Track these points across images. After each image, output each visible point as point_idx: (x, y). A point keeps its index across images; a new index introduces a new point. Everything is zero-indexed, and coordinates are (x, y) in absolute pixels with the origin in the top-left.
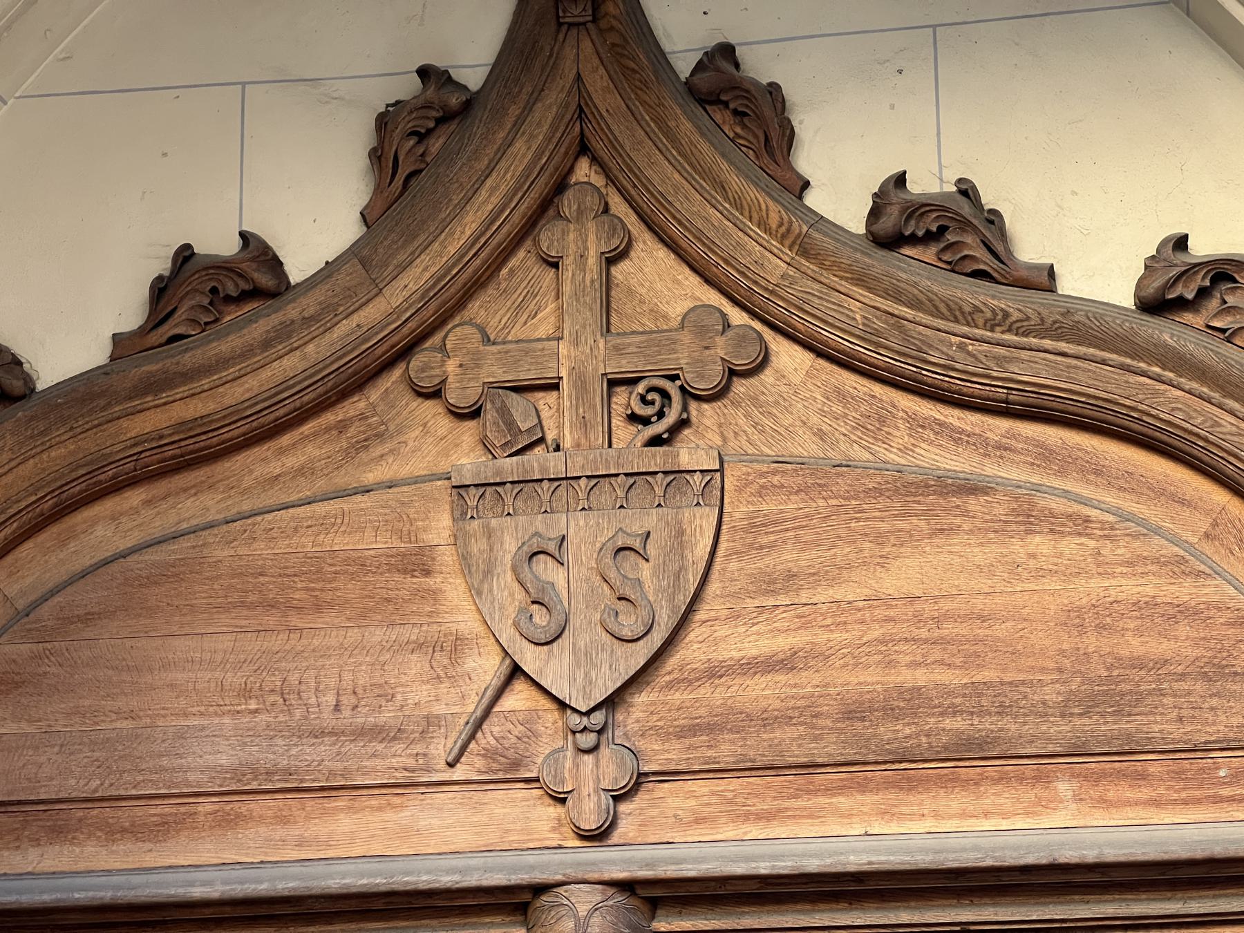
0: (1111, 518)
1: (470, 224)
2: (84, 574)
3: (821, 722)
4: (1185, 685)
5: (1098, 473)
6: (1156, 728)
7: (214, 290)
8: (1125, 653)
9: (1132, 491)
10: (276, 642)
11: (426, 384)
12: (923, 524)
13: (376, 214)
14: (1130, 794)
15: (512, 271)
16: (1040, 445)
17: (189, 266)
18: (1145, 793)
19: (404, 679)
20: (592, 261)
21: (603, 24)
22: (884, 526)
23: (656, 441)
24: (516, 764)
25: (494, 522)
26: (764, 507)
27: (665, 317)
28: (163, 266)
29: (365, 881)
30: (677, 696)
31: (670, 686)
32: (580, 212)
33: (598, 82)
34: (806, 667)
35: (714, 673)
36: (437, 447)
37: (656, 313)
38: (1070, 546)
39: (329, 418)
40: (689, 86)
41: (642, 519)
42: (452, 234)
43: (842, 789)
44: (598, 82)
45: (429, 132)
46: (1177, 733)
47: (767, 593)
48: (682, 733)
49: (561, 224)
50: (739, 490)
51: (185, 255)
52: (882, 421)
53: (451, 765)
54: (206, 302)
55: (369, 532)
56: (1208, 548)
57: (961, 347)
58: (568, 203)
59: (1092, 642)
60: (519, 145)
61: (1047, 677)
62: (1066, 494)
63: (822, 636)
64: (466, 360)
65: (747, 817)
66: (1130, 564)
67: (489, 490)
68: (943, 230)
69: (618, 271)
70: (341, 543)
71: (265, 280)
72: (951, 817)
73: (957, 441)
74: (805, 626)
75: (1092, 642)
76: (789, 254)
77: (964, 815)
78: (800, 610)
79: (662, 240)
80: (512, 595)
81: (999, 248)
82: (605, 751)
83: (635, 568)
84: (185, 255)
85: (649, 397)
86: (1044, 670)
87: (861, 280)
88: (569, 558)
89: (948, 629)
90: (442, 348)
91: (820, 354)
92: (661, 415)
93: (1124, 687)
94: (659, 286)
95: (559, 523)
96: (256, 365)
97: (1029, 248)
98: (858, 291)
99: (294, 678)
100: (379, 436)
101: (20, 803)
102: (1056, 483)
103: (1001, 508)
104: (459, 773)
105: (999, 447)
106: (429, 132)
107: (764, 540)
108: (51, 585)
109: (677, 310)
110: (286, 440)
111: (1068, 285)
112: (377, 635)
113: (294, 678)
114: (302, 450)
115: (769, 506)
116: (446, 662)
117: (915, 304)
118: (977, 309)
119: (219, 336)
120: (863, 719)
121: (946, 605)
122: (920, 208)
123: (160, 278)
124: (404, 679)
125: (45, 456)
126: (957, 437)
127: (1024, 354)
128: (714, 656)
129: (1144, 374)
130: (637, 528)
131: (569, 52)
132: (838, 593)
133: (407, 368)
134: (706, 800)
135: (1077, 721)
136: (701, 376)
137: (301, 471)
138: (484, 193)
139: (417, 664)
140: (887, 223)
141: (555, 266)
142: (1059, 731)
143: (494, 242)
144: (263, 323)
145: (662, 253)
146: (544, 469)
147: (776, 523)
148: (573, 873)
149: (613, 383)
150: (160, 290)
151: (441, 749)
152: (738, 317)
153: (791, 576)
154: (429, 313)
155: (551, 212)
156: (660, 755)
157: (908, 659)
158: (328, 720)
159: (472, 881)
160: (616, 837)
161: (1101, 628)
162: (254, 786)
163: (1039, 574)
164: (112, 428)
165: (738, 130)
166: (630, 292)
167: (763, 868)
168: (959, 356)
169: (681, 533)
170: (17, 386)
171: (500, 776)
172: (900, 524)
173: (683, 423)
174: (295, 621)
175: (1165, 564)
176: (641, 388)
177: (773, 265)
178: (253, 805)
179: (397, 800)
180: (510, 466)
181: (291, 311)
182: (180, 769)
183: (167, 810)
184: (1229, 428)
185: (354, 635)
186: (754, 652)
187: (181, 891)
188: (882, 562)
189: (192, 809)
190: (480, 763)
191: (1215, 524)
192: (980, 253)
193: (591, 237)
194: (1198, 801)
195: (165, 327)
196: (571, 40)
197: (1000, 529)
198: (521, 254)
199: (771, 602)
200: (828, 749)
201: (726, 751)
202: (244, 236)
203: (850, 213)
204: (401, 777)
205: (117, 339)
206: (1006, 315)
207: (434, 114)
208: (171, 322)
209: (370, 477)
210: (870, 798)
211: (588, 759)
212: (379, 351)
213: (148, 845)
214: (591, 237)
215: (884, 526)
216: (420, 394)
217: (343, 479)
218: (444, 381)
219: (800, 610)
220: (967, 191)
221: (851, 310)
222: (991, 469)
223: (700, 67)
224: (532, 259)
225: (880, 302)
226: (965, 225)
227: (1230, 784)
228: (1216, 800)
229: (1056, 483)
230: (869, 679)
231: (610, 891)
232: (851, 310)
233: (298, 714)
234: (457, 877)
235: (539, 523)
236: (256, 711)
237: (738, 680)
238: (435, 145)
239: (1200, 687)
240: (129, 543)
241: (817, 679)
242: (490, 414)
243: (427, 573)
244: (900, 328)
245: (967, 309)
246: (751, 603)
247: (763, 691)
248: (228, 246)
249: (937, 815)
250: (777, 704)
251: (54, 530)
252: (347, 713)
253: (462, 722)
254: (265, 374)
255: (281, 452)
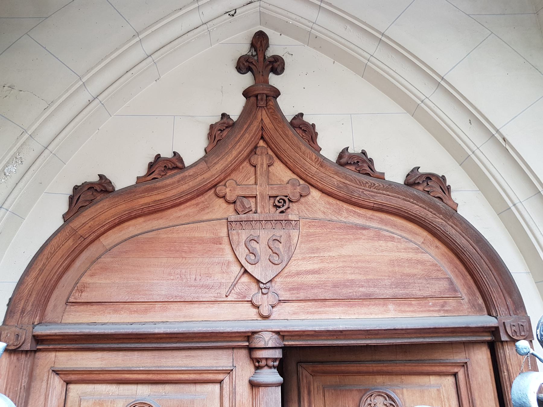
0: (400, 237)
1: (234, 153)
2: (126, 240)
3: (327, 288)
4: (421, 281)
5: (395, 226)
6: (414, 292)
7: (165, 167)
8: (405, 272)
9: (404, 231)
10: (179, 261)
11: (221, 195)
12: (352, 237)
13: (209, 149)
14: (408, 309)
15: (243, 168)
16: (380, 218)
17: (160, 159)
18: (411, 309)
19: (214, 272)
20: (265, 166)
21: (268, 107)
22: (342, 237)
23: (282, 212)
24: (245, 297)
25: (240, 231)
26: (310, 231)
27: (283, 181)
28: (152, 160)
29: (205, 329)
30: (288, 280)
31: (286, 277)
32: (262, 153)
33: (267, 121)
34: (323, 273)
35: (298, 274)
36: (221, 210)
37: (280, 180)
38: (390, 244)
39: (193, 202)
40: (291, 123)
41: (279, 233)
42: (229, 156)
43: (334, 306)
44: (267, 121)
45: (224, 130)
46: (419, 294)
47: (312, 253)
48: (291, 289)
49: (256, 156)
50: (304, 226)
51: (158, 157)
52: (340, 210)
53: (227, 296)
54: (163, 169)
55: (205, 232)
56: (423, 246)
57: (362, 192)
58: (258, 151)
59: (397, 269)
60: (247, 135)
61: (386, 278)
62: (387, 231)
63: (327, 265)
64: (232, 189)
65: (308, 313)
66: (405, 249)
67: (238, 223)
68: (358, 162)
69: (270, 169)
70: (197, 235)
71: (179, 165)
72: (362, 314)
73: (359, 216)
74: (322, 262)
75: (397, 269)
76: (317, 166)
77: (365, 314)
78: (321, 258)
79: (282, 162)
80: (245, 251)
81: (372, 167)
82: (269, 294)
83: (278, 245)
84: (158, 157)
85: (280, 201)
86: (386, 276)
87: (336, 173)
88: (260, 242)
89: (360, 264)
90: (225, 185)
91: (323, 192)
92: (283, 206)
93: (405, 281)
94: (281, 173)
95: (257, 232)
96: (173, 186)
97: (378, 168)
98: (335, 177)
99: (183, 271)
100: (207, 207)
101: (105, 302)
102: (384, 228)
103: (372, 234)
104: (229, 298)
105: (370, 218)
106: (224, 130)
107: (311, 239)
108: (116, 243)
109: (286, 179)
110: (182, 207)
111: (387, 178)
112: (207, 260)
113: (183, 271)
114: (187, 211)
115: (312, 230)
116: (226, 268)
117: (351, 181)
118: (367, 183)
119: (166, 178)
120: (338, 287)
121: (359, 258)
122: (352, 156)
123: (151, 162)
124: (214, 272)
125: (117, 208)
126: (359, 215)
127: (378, 195)
128: (298, 269)
129: (409, 201)
130: (278, 234)
131: (260, 114)
132: (331, 254)
133: (216, 190)
134: (296, 308)
135: (394, 290)
136: (293, 196)
137: (186, 215)
138: (237, 147)
139: (217, 269)
140: (343, 160)
141: (255, 166)
142: (389, 292)
143: (240, 159)
144: (174, 178)
145: (282, 165)
146: (253, 218)
147: (314, 235)
148: (263, 328)
149: (270, 197)
150: (151, 166)
151: (224, 292)
152: (302, 182)
153: (318, 249)
154: (222, 176)
155: (253, 153)
156: (284, 295)
157: (350, 272)
158: (193, 282)
159: (235, 330)
160: (272, 317)
161: (399, 265)
162: (172, 300)
163: (382, 251)
164: (136, 201)
165: (304, 134)
166: (273, 174)
167: (317, 329)
168: (362, 194)
169: (290, 236)
170: (110, 189)
171: (241, 300)
172: (346, 237)
173: (289, 208)
174: (184, 255)
175: (414, 250)
176: (278, 198)
177: (314, 169)
178: (171, 305)
179: (212, 305)
180: (243, 217)
181: (186, 173)
182: (151, 294)
183: (147, 306)
184: (430, 216)
185: (200, 260)
186: (309, 268)
187: (152, 330)
188: (342, 246)
189: (154, 306)
190: (235, 296)
191: (425, 240)
192: (368, 169)
193: (265, 160)
194: (425, 311)
195: (152, 175)
196: (260, 111)
197: (372, 239)
198: (245, 163)
199: (313, 255)
200: (328, 296)
201: (302, 295)
202: (174, 153)
203: (333, 158)
204: (213, 299)
205: (138, 178)
206: (375, 185)
207: (226, 125)
208: (153, 174)
209: (205, 218)
210: (341, 309)
211: (266, 296)
212: (209, 185)
213: (142, 316)
214: (265, 160)
215: (342, 237)
216: (218, 197)
217: (197, 218)
218: (226, 194)
219: (321, 258)
220: (364, 153)
221: (334, 181)
222: (368, 223)
223: (294, 118)
224: (248, 165)
225: (341, 180)
226: (364, 161)
227: (433, 307)
228: (429, 311)
229: (384, 228)
230: (339, 277)
231: (274, 334)
232: (334, 181)
233: (184, 281)
234: (231, 329)
235: (252, 232)
236: (173, 279)
237: (305, 276)
238: (225, 133)
239: (424, 282)
240: (139, 232)
241: (326, 276)
242: (238, 203)
243: (221, 244)
244: (347, 187)
245: (364, 182)
246: (307, 255)
247: (311, 279)
248: (169, 155)
249: (358, 313)
250: (315, 283)
251: (118, 228)
252: (198, 281)
253: (230, 284)
254: (178, 189)
255: (181, 210)
